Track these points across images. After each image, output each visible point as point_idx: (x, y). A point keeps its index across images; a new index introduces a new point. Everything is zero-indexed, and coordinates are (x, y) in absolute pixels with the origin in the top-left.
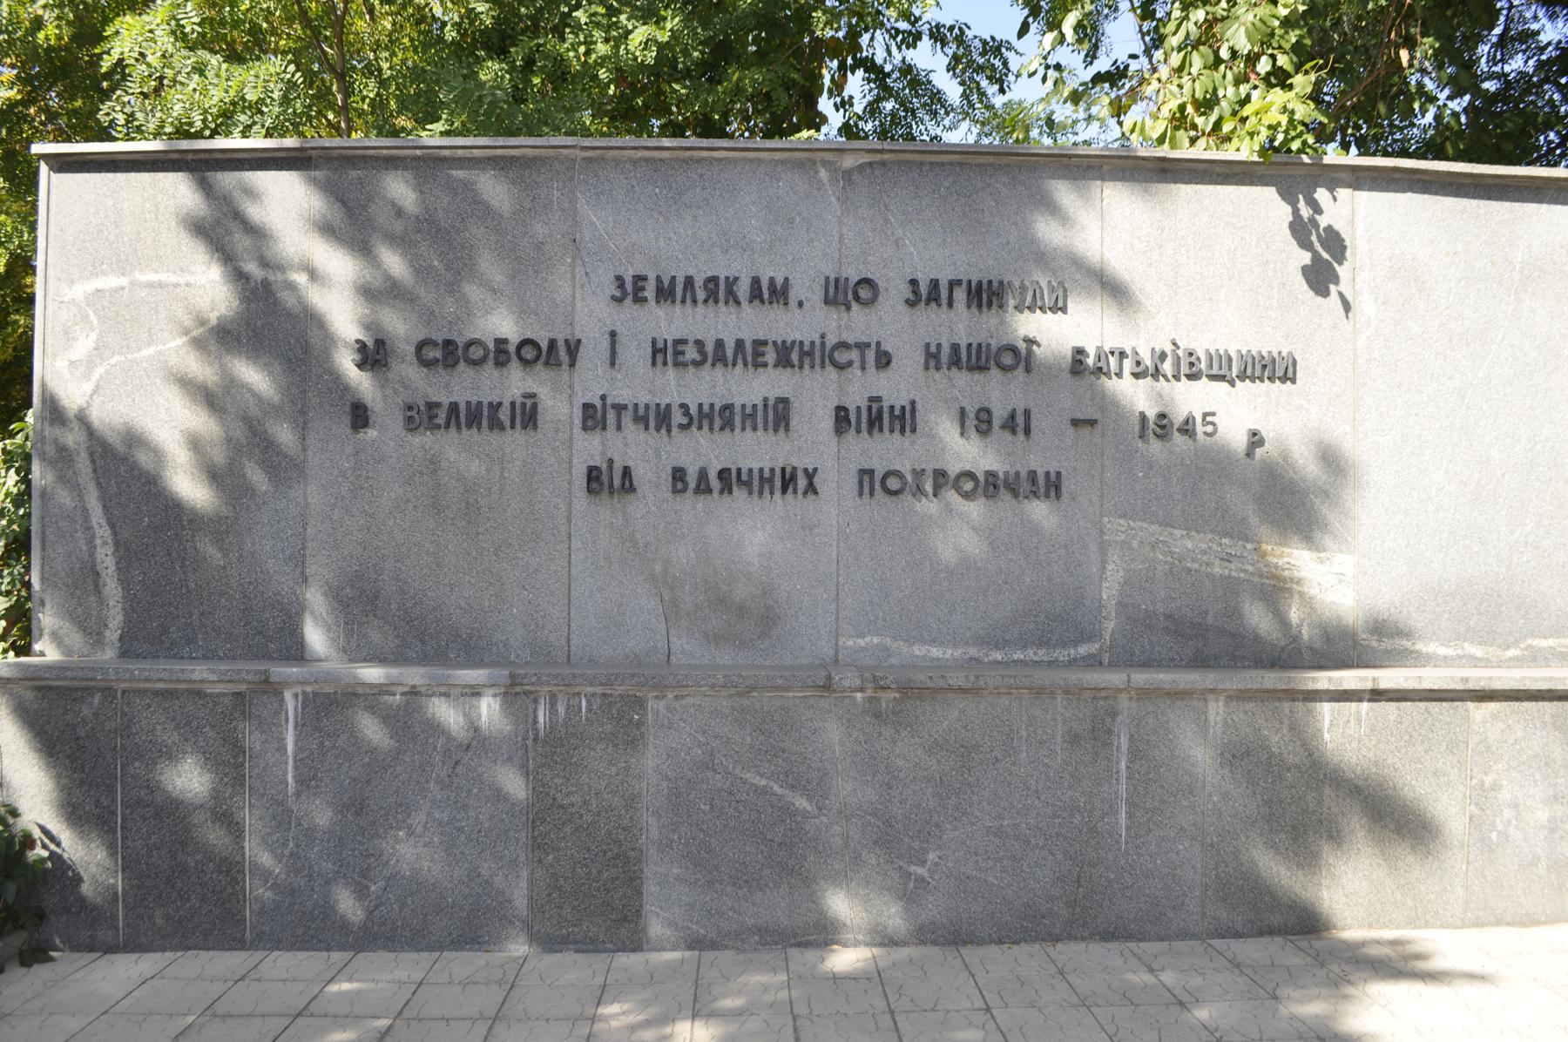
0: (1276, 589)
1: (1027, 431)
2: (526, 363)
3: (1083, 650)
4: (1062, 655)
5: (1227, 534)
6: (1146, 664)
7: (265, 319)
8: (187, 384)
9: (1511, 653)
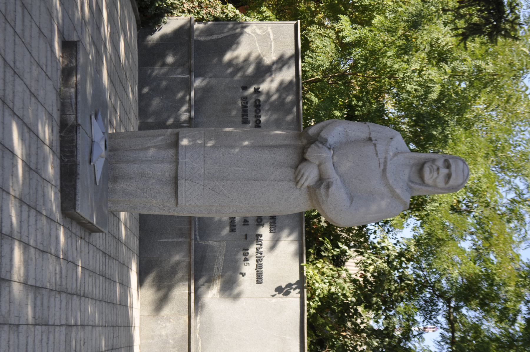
0: (210, 281)
1: (244, 225)
2: (256, 122)
3: (198, 237)
4: (197, 233)
5: (223, 268)
6: (195, 251)
7: (263, 71)
8: (249, 55)
9: (198, 335)
